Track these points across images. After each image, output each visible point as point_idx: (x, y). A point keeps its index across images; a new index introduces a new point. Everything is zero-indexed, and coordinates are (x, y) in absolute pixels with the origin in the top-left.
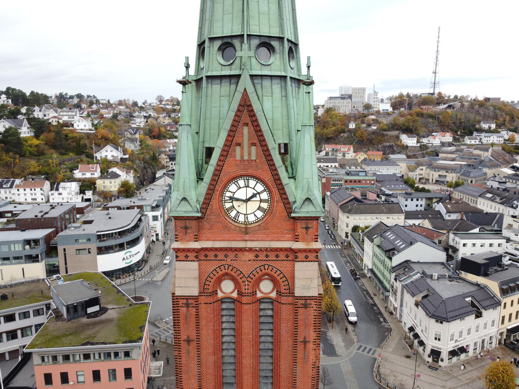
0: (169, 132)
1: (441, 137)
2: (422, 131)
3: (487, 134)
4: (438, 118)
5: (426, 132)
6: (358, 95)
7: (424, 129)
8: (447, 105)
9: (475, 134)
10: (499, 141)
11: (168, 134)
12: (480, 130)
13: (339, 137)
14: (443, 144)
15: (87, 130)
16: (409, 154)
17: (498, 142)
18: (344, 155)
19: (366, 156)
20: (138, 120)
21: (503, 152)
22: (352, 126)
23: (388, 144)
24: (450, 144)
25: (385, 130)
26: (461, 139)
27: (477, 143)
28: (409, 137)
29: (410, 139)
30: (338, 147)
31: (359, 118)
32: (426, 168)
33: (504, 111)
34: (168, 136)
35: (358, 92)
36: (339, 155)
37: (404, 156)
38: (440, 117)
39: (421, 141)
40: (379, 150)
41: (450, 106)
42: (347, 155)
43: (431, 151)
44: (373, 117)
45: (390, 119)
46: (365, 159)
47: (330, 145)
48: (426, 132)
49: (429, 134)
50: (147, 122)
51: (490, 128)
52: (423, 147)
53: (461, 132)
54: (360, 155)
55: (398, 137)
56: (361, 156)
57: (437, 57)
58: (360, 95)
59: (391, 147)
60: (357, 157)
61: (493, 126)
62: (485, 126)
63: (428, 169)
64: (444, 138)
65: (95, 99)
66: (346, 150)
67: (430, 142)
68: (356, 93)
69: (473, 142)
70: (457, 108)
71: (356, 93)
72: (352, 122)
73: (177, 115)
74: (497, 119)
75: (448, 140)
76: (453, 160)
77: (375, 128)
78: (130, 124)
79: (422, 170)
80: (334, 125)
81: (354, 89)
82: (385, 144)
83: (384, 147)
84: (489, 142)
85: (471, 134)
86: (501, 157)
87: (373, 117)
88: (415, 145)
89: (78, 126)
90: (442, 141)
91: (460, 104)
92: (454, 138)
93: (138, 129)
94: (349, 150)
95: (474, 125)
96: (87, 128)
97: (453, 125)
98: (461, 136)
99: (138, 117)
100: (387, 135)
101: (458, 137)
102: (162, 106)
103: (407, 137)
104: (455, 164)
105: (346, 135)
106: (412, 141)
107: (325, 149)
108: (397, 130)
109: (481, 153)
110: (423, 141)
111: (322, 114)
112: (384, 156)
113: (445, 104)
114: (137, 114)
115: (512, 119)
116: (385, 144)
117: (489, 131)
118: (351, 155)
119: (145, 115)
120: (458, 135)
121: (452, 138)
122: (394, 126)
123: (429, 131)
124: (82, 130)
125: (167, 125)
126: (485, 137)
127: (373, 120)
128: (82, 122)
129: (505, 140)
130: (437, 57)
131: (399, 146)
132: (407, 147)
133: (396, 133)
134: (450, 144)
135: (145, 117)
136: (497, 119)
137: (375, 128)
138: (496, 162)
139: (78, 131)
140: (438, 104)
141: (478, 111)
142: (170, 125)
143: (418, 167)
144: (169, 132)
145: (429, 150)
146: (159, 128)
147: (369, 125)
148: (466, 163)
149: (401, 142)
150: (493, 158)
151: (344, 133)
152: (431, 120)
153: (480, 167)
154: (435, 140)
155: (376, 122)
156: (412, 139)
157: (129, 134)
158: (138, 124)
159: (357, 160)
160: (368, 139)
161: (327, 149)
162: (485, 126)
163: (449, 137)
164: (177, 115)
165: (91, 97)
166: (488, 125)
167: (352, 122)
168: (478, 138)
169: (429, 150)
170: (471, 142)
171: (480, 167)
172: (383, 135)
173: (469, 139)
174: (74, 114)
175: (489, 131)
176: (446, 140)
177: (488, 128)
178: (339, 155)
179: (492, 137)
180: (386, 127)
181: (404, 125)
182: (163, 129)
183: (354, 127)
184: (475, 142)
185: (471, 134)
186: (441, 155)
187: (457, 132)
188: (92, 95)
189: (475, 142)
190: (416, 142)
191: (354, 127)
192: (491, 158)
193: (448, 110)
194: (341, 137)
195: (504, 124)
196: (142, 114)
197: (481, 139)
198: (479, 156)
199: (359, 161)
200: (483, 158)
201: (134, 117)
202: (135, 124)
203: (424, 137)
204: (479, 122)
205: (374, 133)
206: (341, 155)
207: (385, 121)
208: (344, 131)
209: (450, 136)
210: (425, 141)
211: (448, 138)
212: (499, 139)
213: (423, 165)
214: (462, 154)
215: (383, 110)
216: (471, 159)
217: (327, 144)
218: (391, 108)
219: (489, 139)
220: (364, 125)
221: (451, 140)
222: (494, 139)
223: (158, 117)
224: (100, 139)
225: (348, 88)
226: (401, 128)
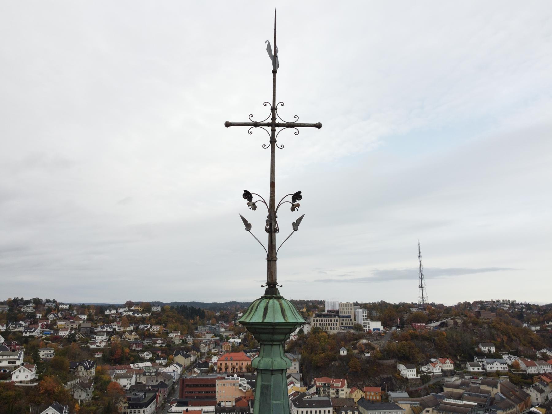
0: (134, 354)
1: (441, 365)
2: (420, 357)
3: (489, 360)
4: (434, 340)
5: (424, 358)
6: (345, 310)
7: (421, 355)
8: (438, 323)
9: (476, 359)
10: (504, 368)
11: (132, 356)
12: (482, 355)
13: (330, 365)
14: (445, 373)
15: (28, 382)
16: (411, 389)
17: (502, 369)
18: (337, 392)
19: (364, 395)
20: (99, 338)
21: (512, 385)
22: (343, 352)
23: (385, 376)
24: (452, 373)
25: (380, 359)
26: (463, 365)
27: (481, 370)
28: (407, 368)
29: (409, 370)
30: (331, 381)
31: (350, 341)
32: (433, 409)
33: (498, 330)
34: (132, 359)
35: (345, 307)
36: (332, 391)
37: (405, 395)
38: (436, 338)
39: (420, 370)
40: (377, 386)
41: (442, 325)
42: (341, 392)
43: (434, 384)
44: (365, 341)
45: (384, 342)
46: (362, 399)
47: (320, 379)
48: (424, 358)
49: (427, 362)
50: (110, 339)
51: (490, 351)
52: (425, 378)
53: (460, 356)
54: (355, 393)
55: (395, 369)
56: (358, 395)
57: (421, 272)
58: (348, 311)
59: (388, 380)
60: (353, 396)
61: (493, 349)
62: (485, 349)
63: (435, 411)
64: (445, 365)
65: (54, 305)
66: (340, 386)
67: (431, 370)
68: (343, 309)
69: (476, 370)
70: (451, 326)
71: (343, 309)
72: (343, 348)
73: (146, 327)
74: (495, 340)
75: (449, 368)
76: (460, 397)
77: (368, 355)
78: (89, 345)
79: (429, 411)
80: (323, 350)
81: (341, 305)
82: (382, 376)
83: (383, 380)
84: (493, 369)
85: (471, 360)
86: (511, 393)
87: (365, 341)
88: (415, 377)
89: (17, 377)
90: (443, 369)
91: (452, 321)
92: (455, 365)
93: (98, 350)
94: (343, 386)
95: (473, 349)
96: (29, 379)
97: (450, 348)
98: (462, 361)
99: (100, 333)
100: (382, 365)
101: (458, 362)
102: (131, 313)
103: (405, 368)
104: (465, 405)
105: (337, 364)
106: (411, 373)
107: (315, 383)
108: (393, 357)
109: (490, 389)
110: (423, 369)
111: (308, 332)
112: (383, 392)
113: (437, 321)
114: (99, 329)
115: (510, 340)
116: (382, 376)
117: (489, 355)
118: (344, 393)
119: (109, 330)
120: (458, 360)
121: (453, 365)
122: (388, 353)
123: (427, 356)
124: (21, 382)
125: (133, 343)
126: (488, 363)
127: (365, 344)
128: (24, 371)
129: (509, 366)
130: (421, 272)
131: (398, 379)
132: (407, 379)
133: (392, 362)
134: (452, 373)
135: (108, 333)
136: (495, 340)
137: (368, 355)
138: (508, 400)
139: (17, 384)
140: (431, 321)
141: (473, 330)
142: (136, 344)
143: (424, 409)
144: (134, 354)
145: (431, 383)
146: (123, 349)
147: (362, 352)
148: (476, 404)
149: (400, 373)
150: (504, 395)
151: (335, 361)
152: (426, 343)
153: (493, 410)
154: (437, 367)
155: (369, 347)
156: (411, 370)
157: (83, 368)
158: (98, 344)
159: (353, 399)
160: (362, 370)
161: (318, 384)
162: (485, 350)
163: (449, 364)
164: (146, 327)
165: (50, 301)
166: (487, 348)
167: (343, 348)
168: (481, 364)
169: (431, 383)
170: (474, 369)
171: (493, 410)
172: (379, 365)
173: (472, 366)
174: (16, 357)
175: (489, 355)
176: (447, 368)
177: (487, 351)
178: (332, 391)
179: (495, 364)
180: (380, 355)
181: (399, 351)
182: (127, 350)
183: (345, 354)
184: (478, 369)
185: (471, 360)
186: (446, 389)
187: (456, 356)
188: (51, 300)
189: (478, 369)
190: (415, 373)
191: (345, 354)
192: (501, 395)
193: (442, 329)
194: (332, 365)
195: (504, 347)
196: (105, 330)
197: (483, 365)
198: (488, 392)
199: (356, 400)
200: (493, 396)
201: (96, 333)
202: (94, 344)
203: (423, 365)
204: (477, 344)
205: (368, 360)
206: (334, 391)
207: (378, 346)
208: (334, 359)
209: (451, 363)
210: (424, 369)
211: (449, 366)
212: (502, 366)
213: (429, 407)
214: (468, 389)
215: (374, 329)
216: (480, 396)
217: (317, 377)
218: (382, 327)
219: (492, 366)
220: (356, 351)
221: (453, 368)
222: (497, 366)
223: (124, 332)
224: (43, 394)
225: (335, 304)
226: (397, 355)
